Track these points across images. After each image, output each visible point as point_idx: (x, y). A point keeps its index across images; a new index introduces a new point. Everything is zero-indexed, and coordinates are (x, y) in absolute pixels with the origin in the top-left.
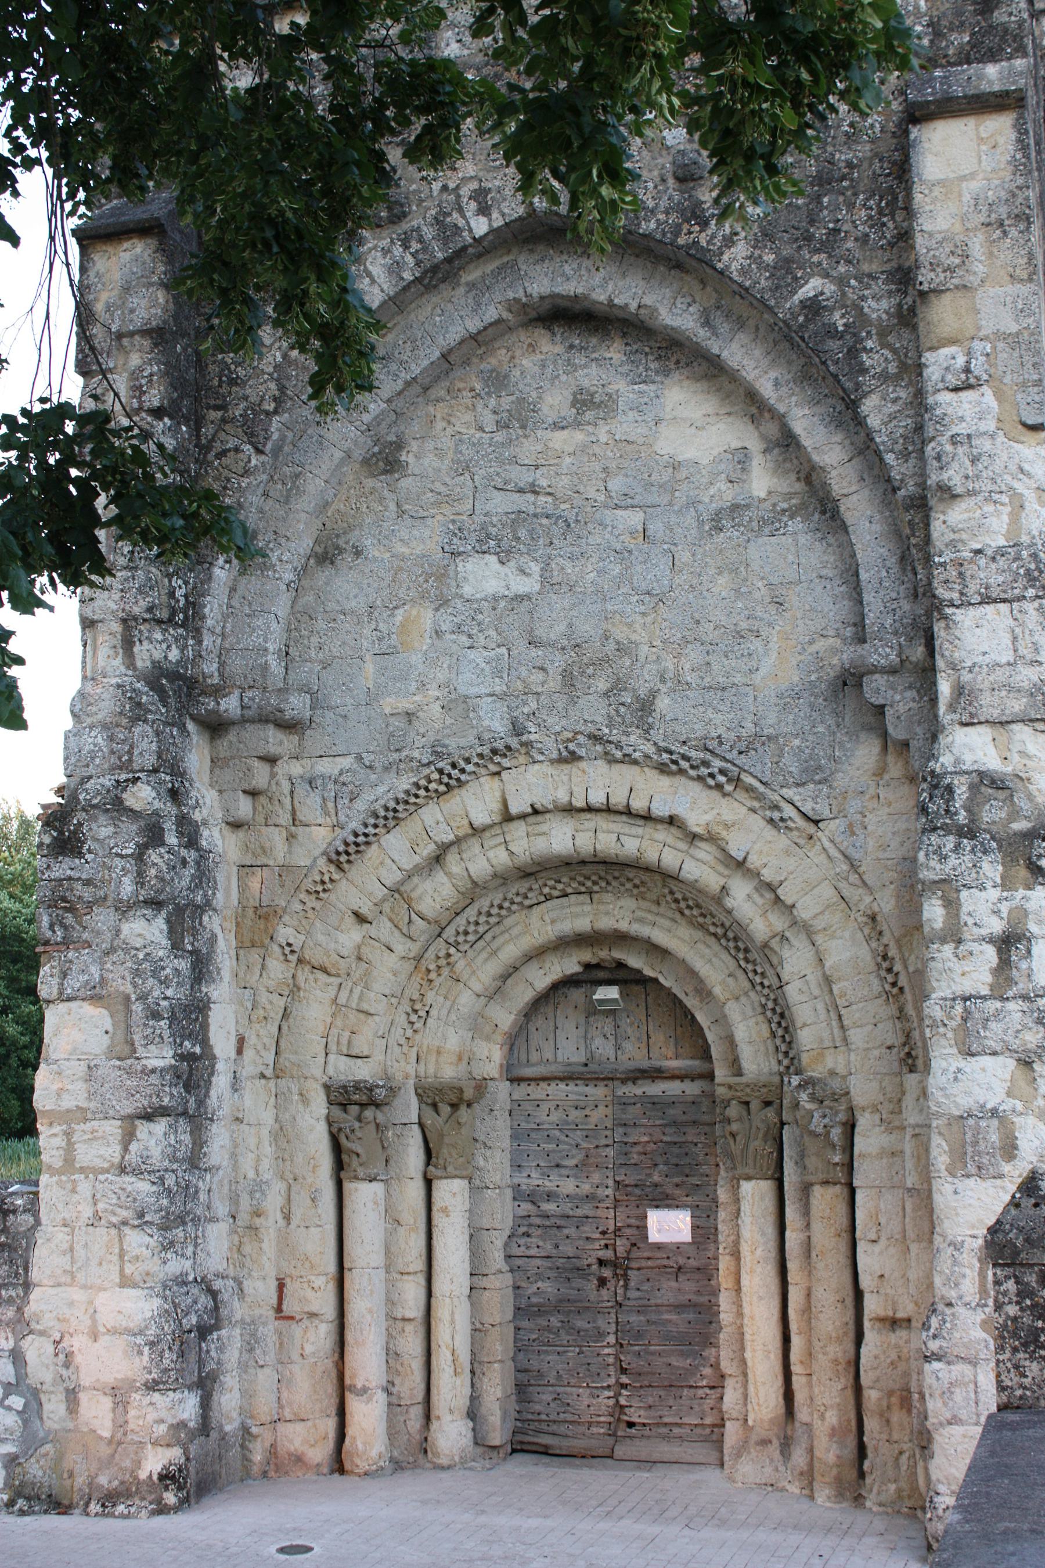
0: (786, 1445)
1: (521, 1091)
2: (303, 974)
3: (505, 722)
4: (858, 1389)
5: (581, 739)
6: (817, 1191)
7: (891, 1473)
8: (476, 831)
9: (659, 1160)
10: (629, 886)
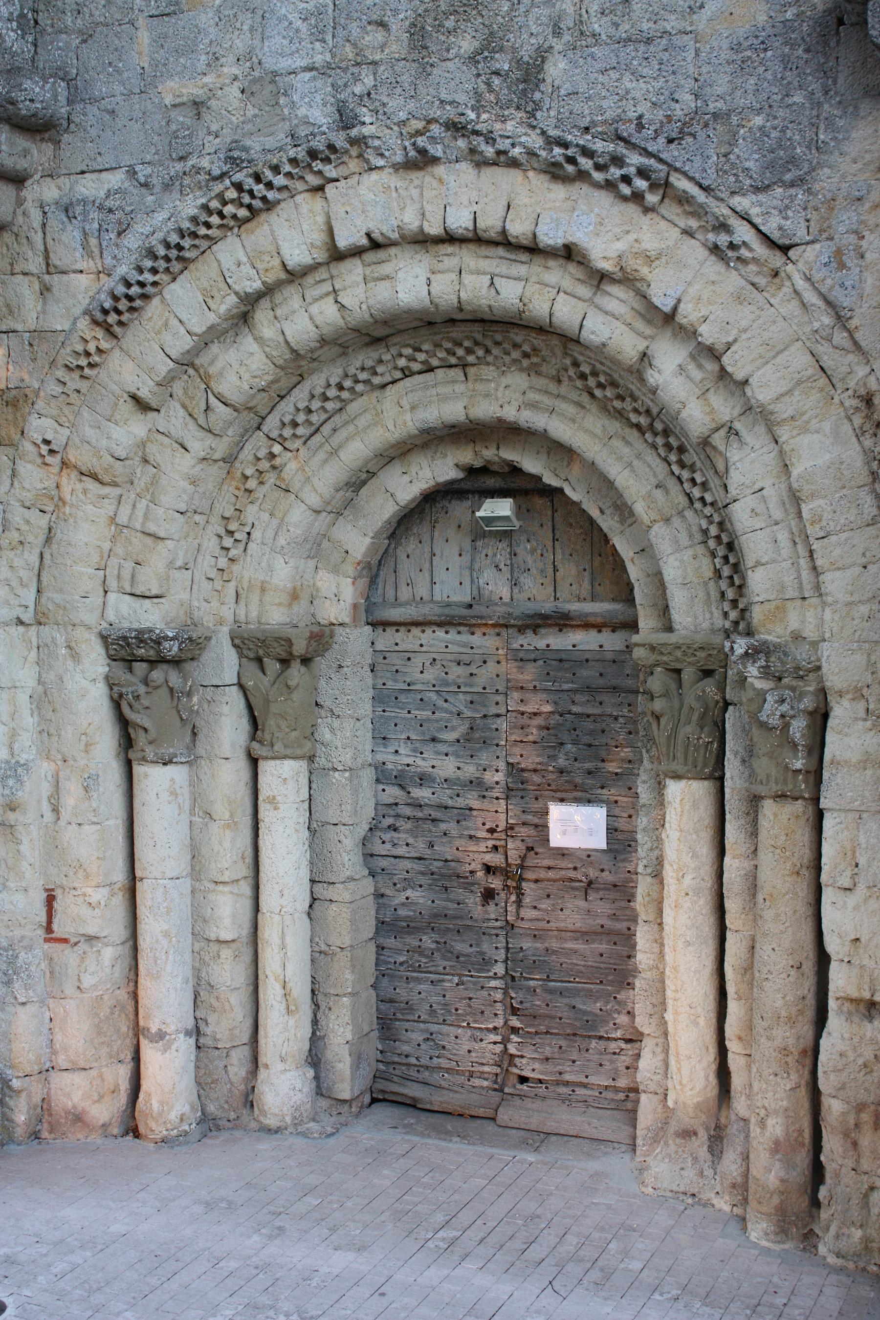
0: (717, 1140)
1: (386, 639)
3: (330, 109)
4: (815, 1094)
5: (436, 129)
6: (768, 808)
7: (855, 1213)
8: (295, 276)
9: (565, 737)
10: (516, 354)
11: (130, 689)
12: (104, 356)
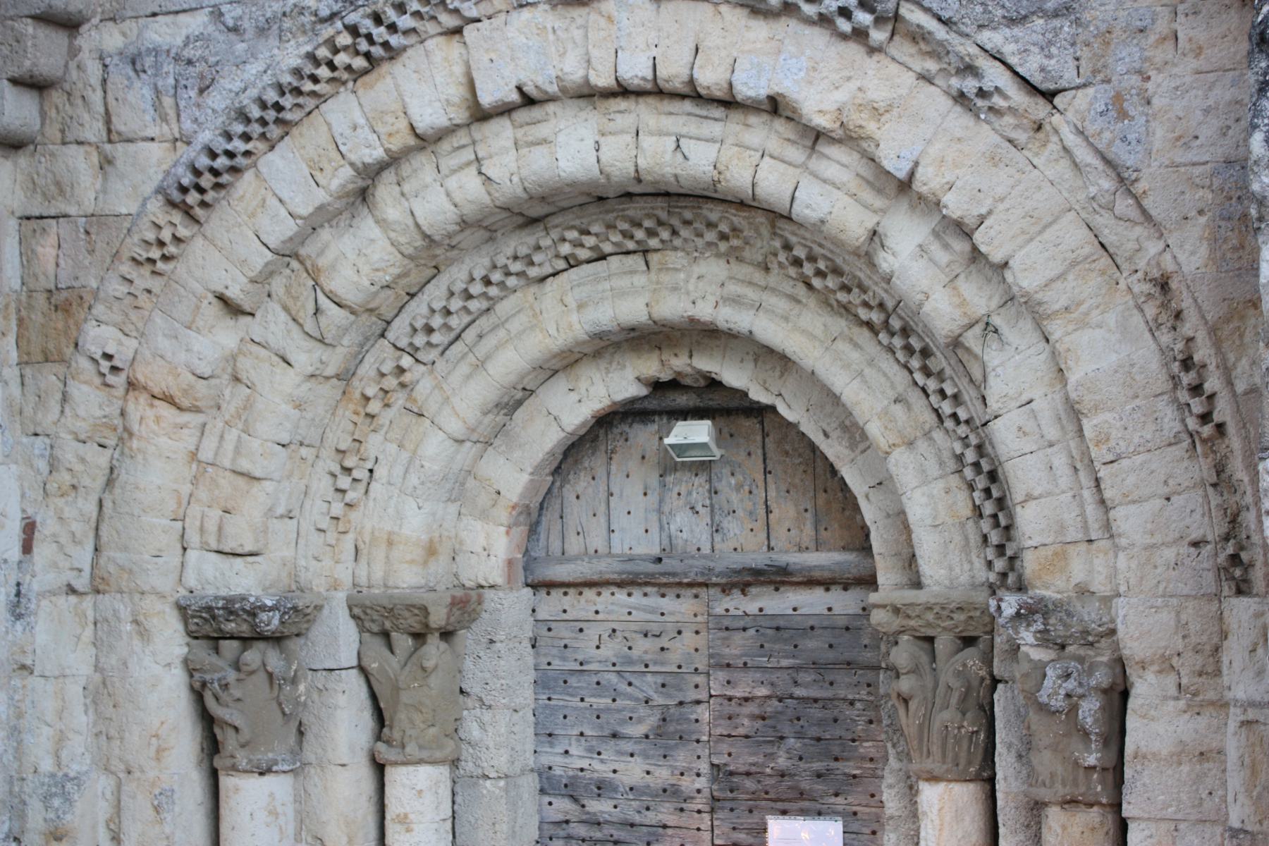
1: (551, 605)
2: (138, 407)
6: (1055, 818)
8: (425, 141)
9: (787, 730)
10: (711, 236)
11: (216, 676)
12: (182, 246)
